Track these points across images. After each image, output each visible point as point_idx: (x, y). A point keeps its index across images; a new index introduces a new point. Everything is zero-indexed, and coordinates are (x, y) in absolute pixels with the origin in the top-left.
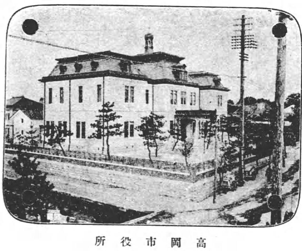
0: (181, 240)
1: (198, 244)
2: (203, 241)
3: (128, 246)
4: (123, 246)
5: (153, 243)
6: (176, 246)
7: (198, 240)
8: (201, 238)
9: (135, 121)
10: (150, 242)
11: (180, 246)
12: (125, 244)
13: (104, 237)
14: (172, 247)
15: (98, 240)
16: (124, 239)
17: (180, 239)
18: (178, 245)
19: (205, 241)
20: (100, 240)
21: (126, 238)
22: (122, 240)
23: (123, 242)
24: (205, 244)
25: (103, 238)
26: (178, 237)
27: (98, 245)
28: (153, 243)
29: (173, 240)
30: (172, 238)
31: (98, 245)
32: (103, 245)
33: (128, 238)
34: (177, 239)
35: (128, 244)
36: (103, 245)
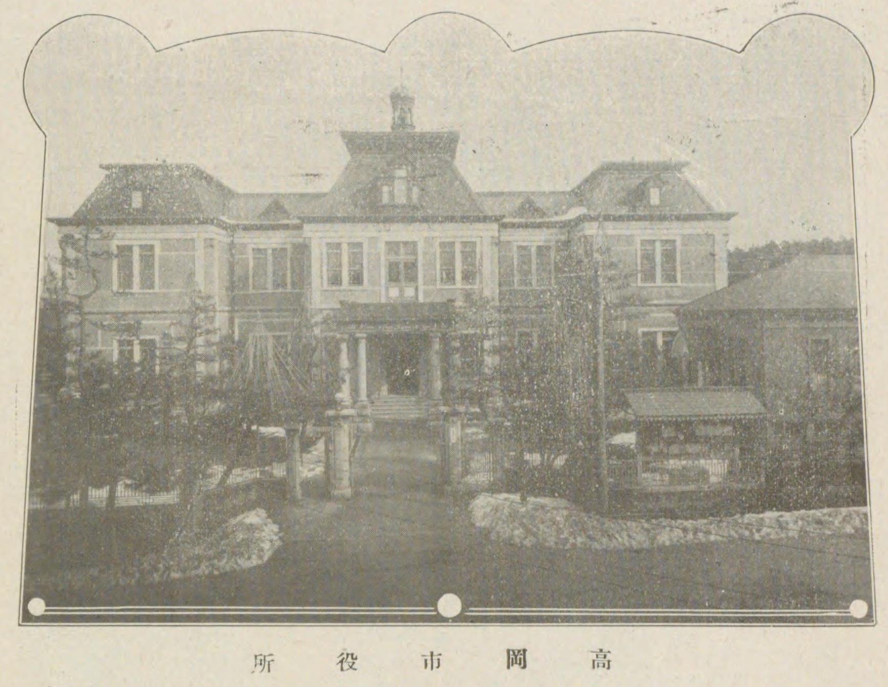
0: (527, 653)
1: (594, 661)
2: (605, 657)
3: (351, 670)
4: (342, 669)
5: (435, 664)
6: (516, 668)
7: (594, 655)
8: (601, 651)
9: (609, 671)
10: (429, 662)
11: (525, 667)
12: (346, 666)
13: (271, 655)
14: (508, 667)
15: (258, 662)
16: (345, 656)
17: (525, 651)
18: (520, 664)
19: (609, 657)
20: (517, 658)
21: (348, 655)
22: (341, 658)
23: (342, 662)
24: (609, 661)
25: (268, 659)
26: (521, 647)
27: (438, 667)
28: (435, 664)
29: (511, 653)
30: (508, 651)
31: (438, 667)
32: (269, 671)
33: (352, 655)
34: (519, 651)
35: (351, 667)
36: (269, 671)
